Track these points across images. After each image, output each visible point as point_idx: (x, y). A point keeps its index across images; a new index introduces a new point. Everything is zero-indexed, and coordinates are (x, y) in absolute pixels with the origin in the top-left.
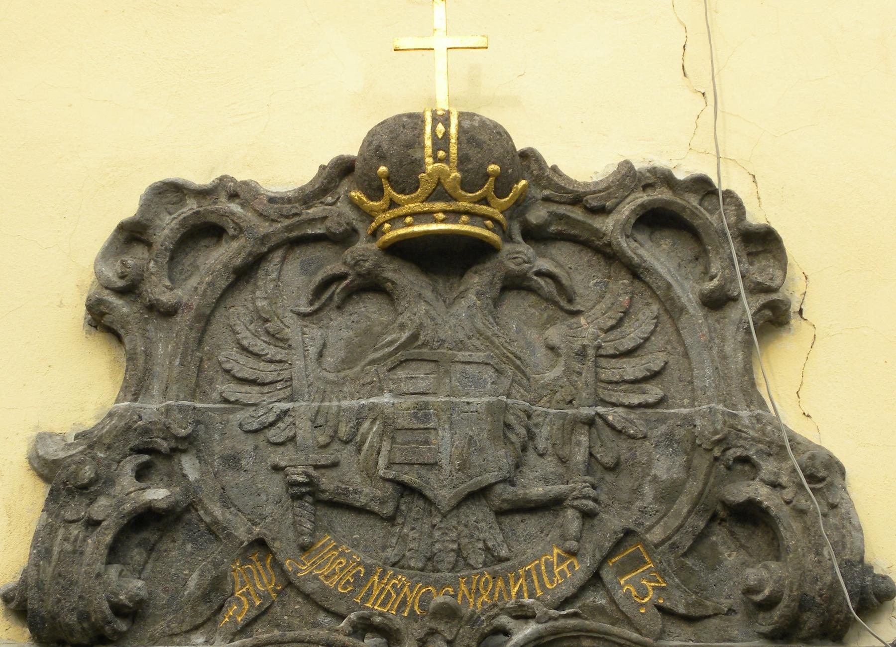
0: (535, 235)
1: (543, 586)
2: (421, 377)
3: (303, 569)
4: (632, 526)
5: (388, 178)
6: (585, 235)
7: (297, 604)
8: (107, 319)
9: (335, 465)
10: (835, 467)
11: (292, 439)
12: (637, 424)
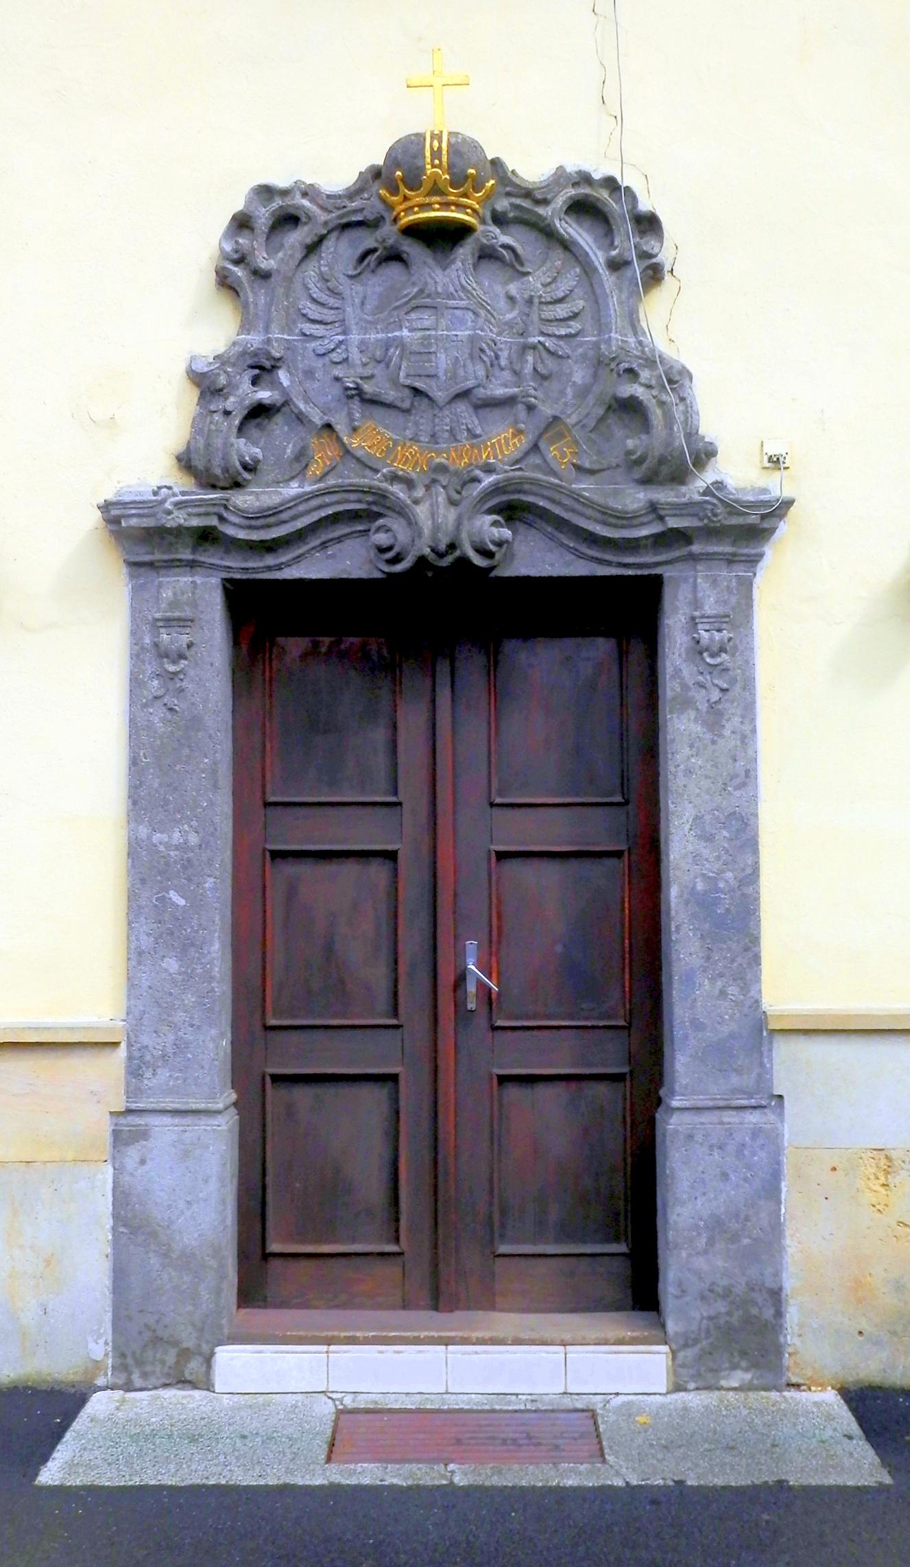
0: (499, 220)
1: (502, 452)
2: (427, 319)
3: (354, 443)
4: (558, 414)
5: (402, 180)
6: (534, 219)
7: (353, 464)
8: (229, 280)
9: (372, 377)
10: (686, 373)
11: (346, 360)
12: (564, 348)
